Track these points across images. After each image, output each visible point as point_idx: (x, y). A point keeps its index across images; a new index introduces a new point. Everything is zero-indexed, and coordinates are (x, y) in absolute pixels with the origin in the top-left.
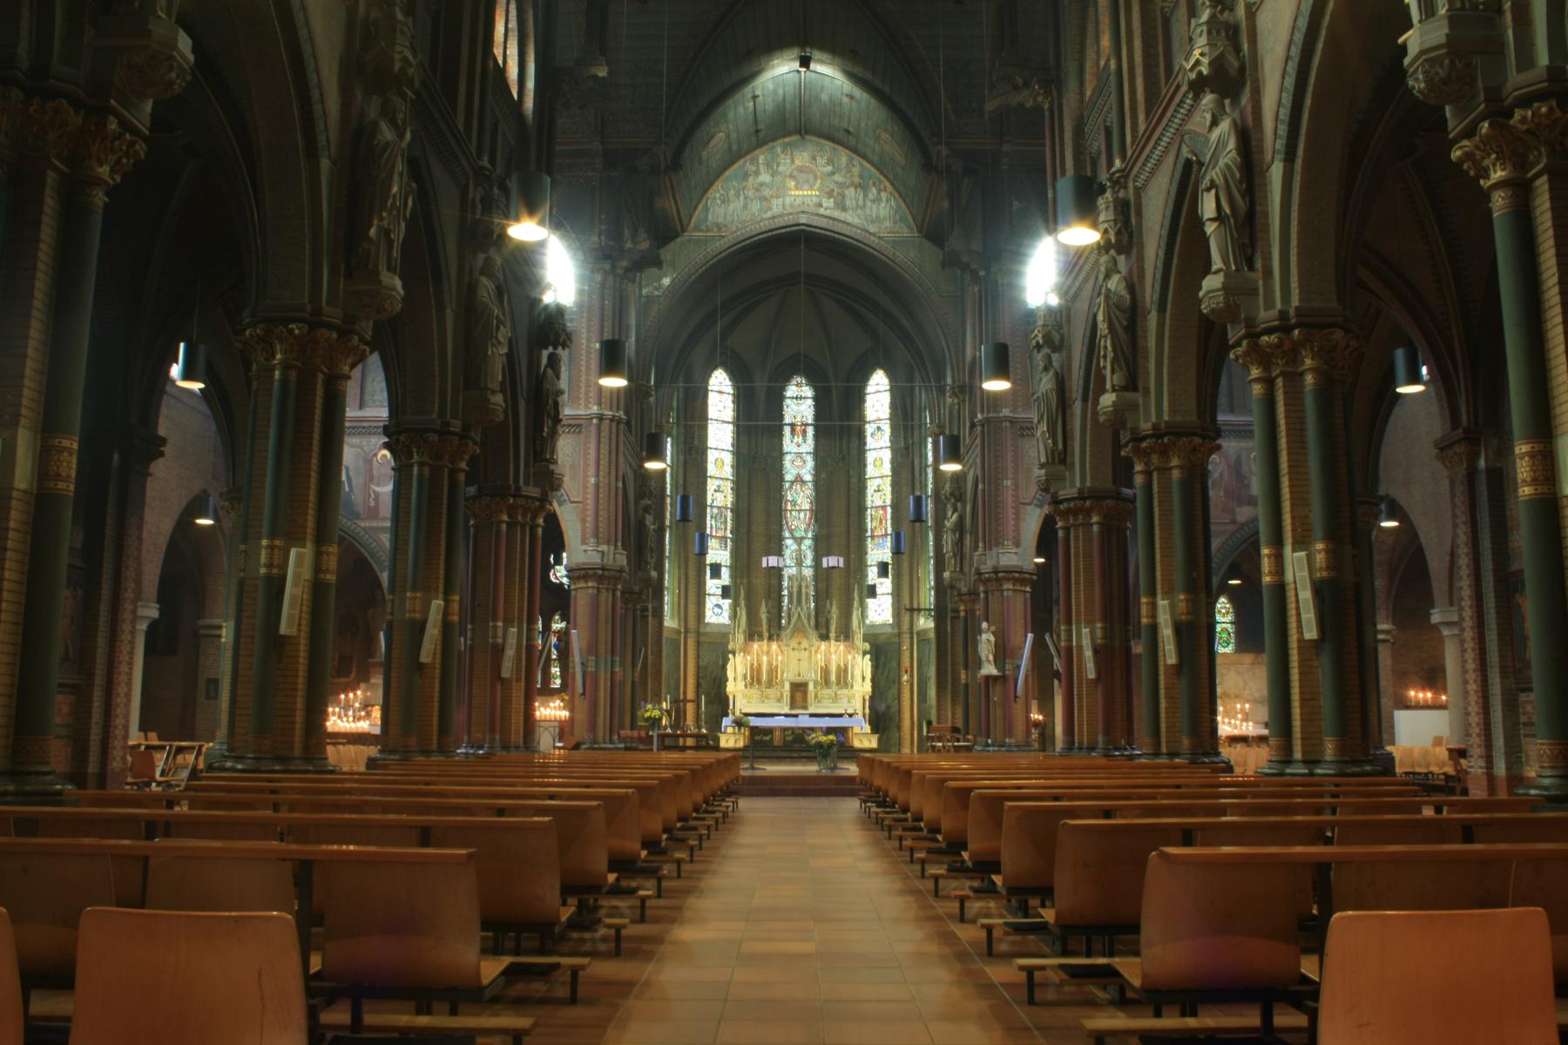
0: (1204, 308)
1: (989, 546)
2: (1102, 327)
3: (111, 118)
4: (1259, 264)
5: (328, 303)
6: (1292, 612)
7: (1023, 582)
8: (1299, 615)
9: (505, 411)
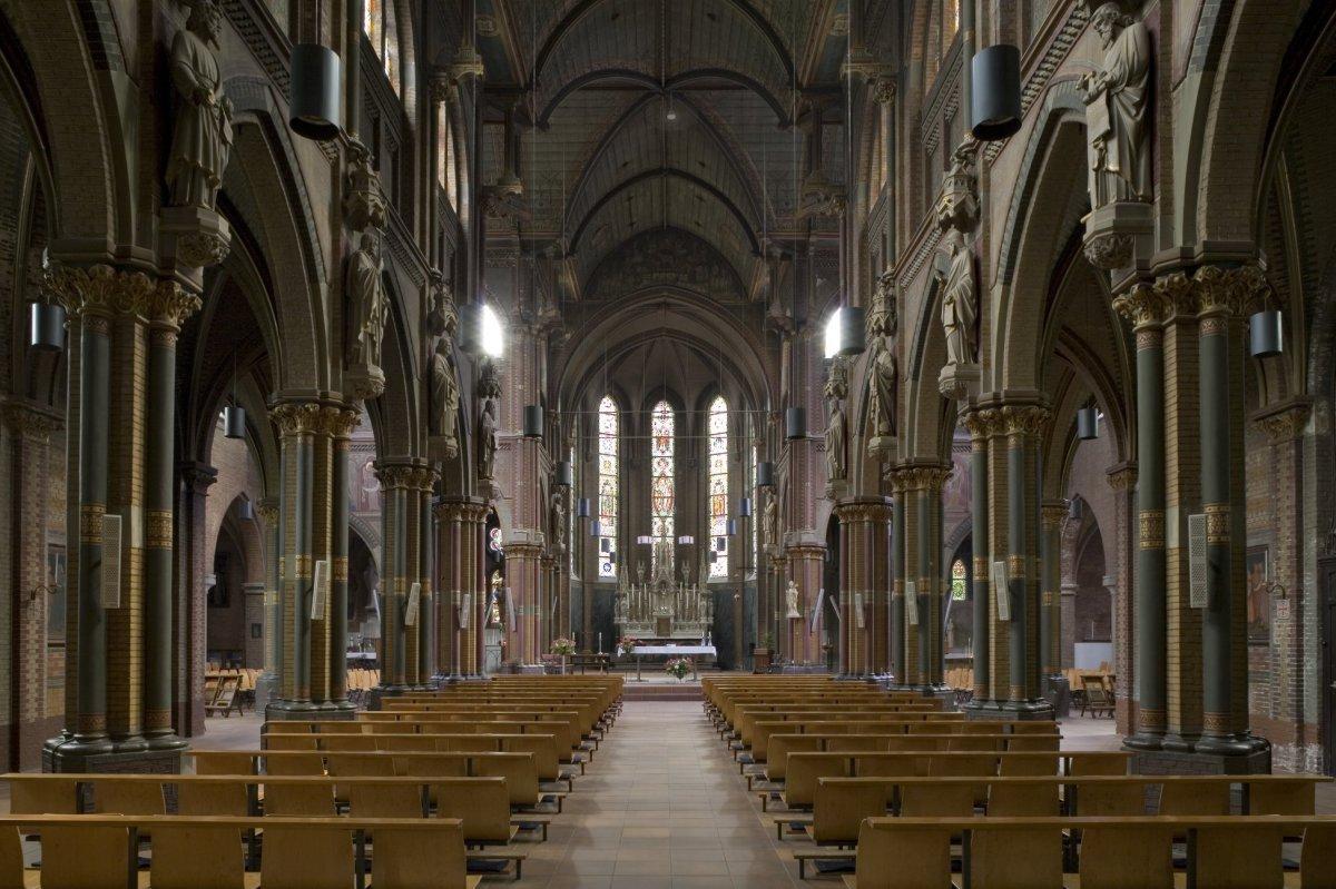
0: (942, 389)
1: (794, 528)
2: (873, 390)
3: (177, 284)
4: (981, 358)
5: (333, 389)
6: (992, 601)
7: (817, 552)
8: (996, 603)
9: (458, 450)
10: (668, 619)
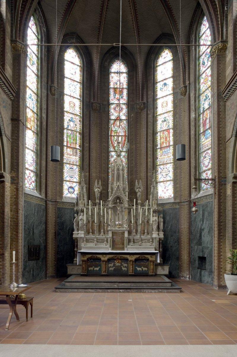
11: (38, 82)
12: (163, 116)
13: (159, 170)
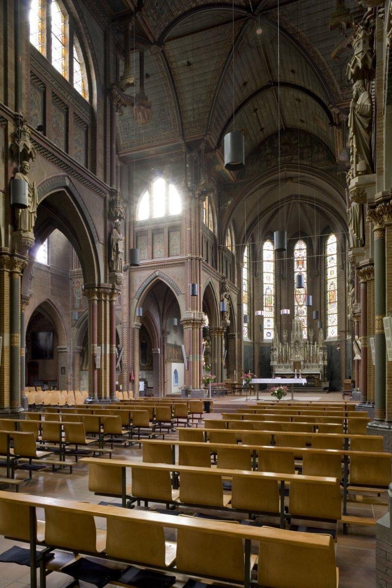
10: (300, 362)
11: (248, 272)
12: (331, 281)
13: (329, 318)
